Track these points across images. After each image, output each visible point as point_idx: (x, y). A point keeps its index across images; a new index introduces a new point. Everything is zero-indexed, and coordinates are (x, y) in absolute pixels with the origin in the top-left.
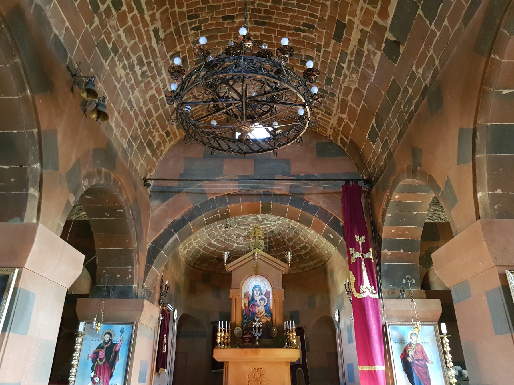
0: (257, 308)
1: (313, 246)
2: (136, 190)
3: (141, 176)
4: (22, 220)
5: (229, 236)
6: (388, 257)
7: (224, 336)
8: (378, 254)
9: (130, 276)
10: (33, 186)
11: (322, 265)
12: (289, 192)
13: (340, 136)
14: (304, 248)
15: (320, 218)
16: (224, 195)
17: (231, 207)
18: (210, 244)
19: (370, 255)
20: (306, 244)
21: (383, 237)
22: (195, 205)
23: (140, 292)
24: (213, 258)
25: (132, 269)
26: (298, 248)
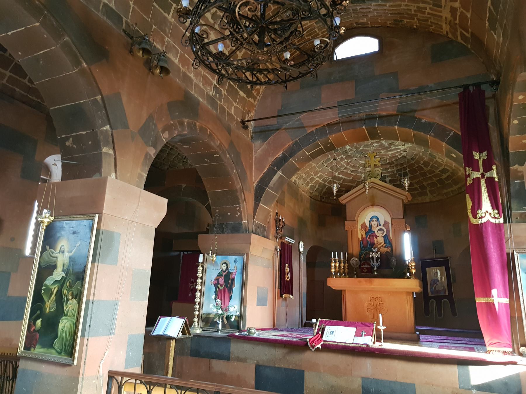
0: (375, 239)
2: (230, 134)
3: (237, 119)
4: (101, 175)
5: (353, 167)
8: (505, 172)
9: (239, 214)
10: (106, 145)
12: (398, 111)
13: (459, 31)
14: (444, 171)
16: (324, 126)
17: (332, 138)
20: (446, 167)
21: (511, 151)
22: (294, 141)
23: (251, 227)
25: (239, 207)
26: (437, 172)
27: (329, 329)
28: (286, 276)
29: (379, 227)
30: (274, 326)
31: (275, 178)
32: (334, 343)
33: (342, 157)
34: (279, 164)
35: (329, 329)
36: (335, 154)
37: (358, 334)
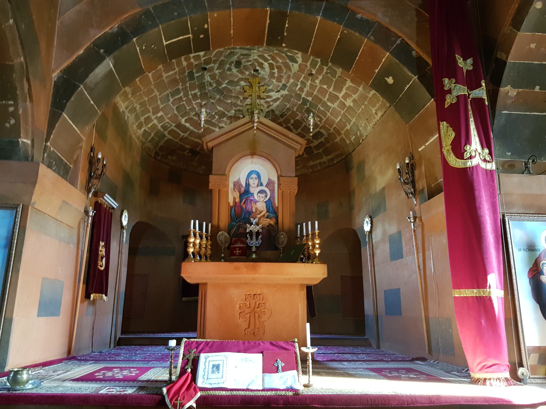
0: (253, 204)
1: (332, 130)
6: (509, 102)
7: (200, 243)
8: (493, 95)
9: (13, 121)
11: (342, 160)
15: (376, 41)
18: (179, 125)
19: (481, 93)
20: (322, 130)
24: (184, 149)
25: (16, 105)
27: (207, 360)
28: (100, 263)
29: (260, 188)
30: (69, 352)
31: (100, 71)
32: (224, 393)
33: (195, 94)
34: (111, 44)
35: (207, 360)
36: (188, 85)
37: (269, 368)
